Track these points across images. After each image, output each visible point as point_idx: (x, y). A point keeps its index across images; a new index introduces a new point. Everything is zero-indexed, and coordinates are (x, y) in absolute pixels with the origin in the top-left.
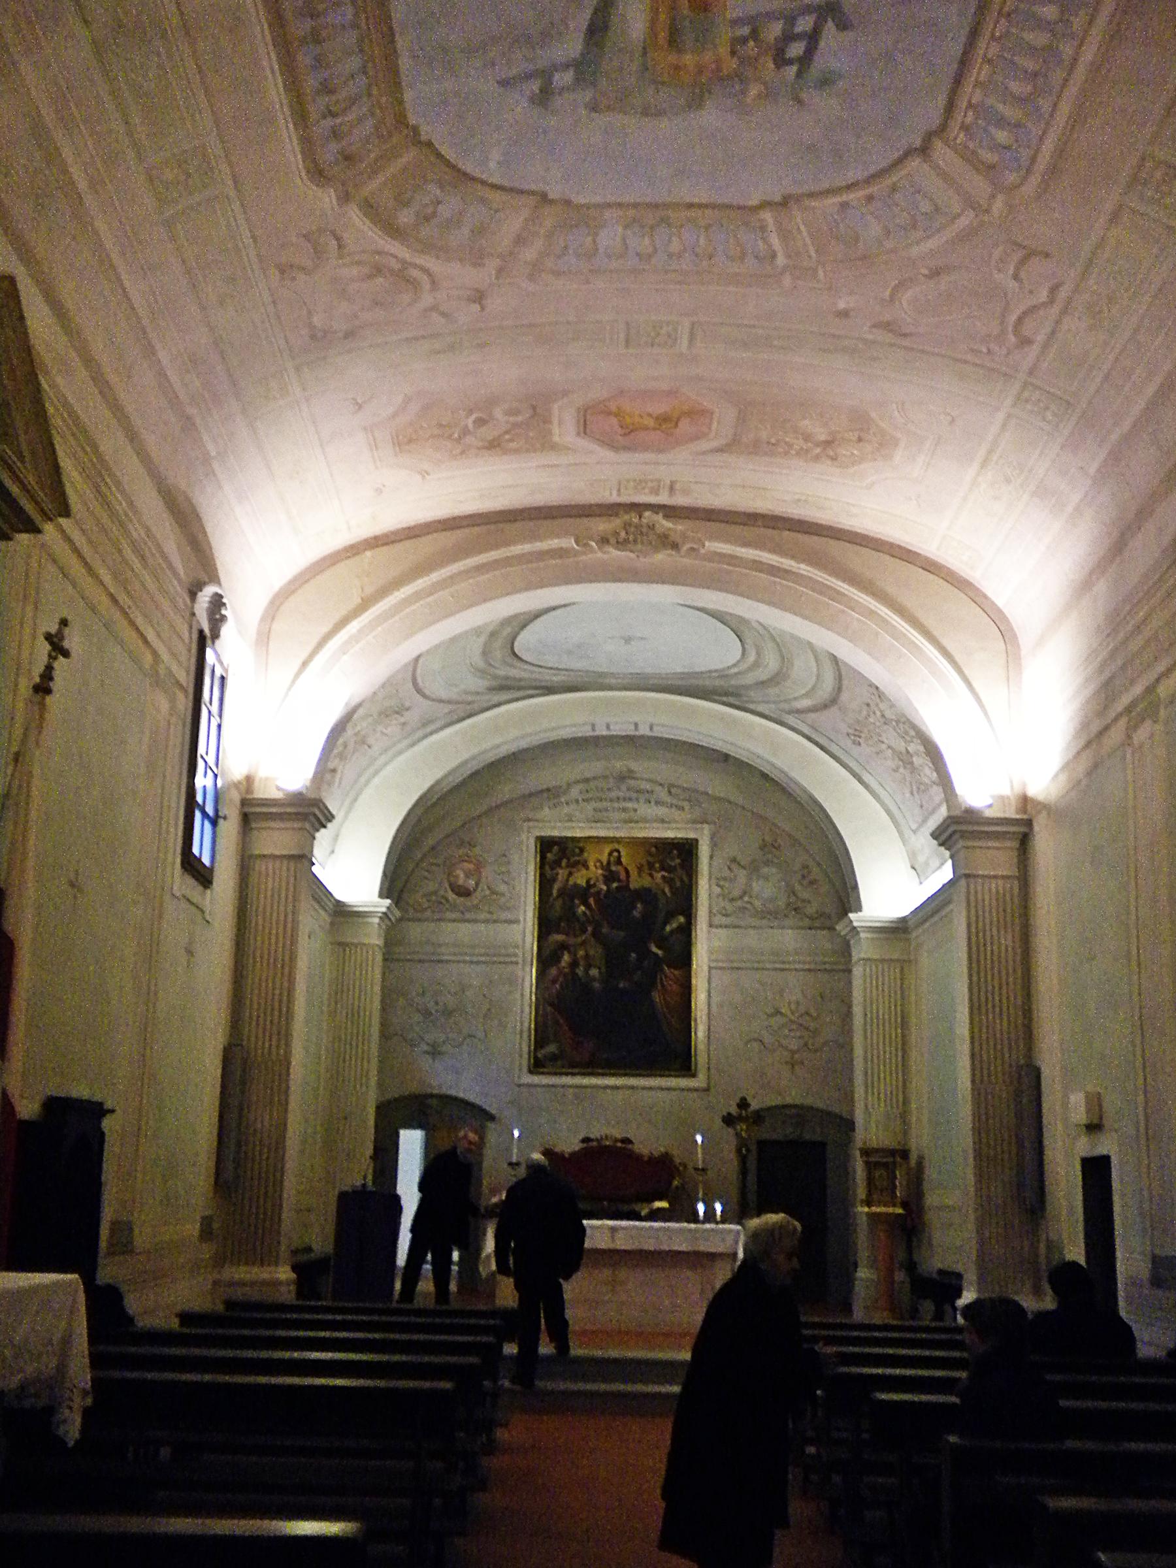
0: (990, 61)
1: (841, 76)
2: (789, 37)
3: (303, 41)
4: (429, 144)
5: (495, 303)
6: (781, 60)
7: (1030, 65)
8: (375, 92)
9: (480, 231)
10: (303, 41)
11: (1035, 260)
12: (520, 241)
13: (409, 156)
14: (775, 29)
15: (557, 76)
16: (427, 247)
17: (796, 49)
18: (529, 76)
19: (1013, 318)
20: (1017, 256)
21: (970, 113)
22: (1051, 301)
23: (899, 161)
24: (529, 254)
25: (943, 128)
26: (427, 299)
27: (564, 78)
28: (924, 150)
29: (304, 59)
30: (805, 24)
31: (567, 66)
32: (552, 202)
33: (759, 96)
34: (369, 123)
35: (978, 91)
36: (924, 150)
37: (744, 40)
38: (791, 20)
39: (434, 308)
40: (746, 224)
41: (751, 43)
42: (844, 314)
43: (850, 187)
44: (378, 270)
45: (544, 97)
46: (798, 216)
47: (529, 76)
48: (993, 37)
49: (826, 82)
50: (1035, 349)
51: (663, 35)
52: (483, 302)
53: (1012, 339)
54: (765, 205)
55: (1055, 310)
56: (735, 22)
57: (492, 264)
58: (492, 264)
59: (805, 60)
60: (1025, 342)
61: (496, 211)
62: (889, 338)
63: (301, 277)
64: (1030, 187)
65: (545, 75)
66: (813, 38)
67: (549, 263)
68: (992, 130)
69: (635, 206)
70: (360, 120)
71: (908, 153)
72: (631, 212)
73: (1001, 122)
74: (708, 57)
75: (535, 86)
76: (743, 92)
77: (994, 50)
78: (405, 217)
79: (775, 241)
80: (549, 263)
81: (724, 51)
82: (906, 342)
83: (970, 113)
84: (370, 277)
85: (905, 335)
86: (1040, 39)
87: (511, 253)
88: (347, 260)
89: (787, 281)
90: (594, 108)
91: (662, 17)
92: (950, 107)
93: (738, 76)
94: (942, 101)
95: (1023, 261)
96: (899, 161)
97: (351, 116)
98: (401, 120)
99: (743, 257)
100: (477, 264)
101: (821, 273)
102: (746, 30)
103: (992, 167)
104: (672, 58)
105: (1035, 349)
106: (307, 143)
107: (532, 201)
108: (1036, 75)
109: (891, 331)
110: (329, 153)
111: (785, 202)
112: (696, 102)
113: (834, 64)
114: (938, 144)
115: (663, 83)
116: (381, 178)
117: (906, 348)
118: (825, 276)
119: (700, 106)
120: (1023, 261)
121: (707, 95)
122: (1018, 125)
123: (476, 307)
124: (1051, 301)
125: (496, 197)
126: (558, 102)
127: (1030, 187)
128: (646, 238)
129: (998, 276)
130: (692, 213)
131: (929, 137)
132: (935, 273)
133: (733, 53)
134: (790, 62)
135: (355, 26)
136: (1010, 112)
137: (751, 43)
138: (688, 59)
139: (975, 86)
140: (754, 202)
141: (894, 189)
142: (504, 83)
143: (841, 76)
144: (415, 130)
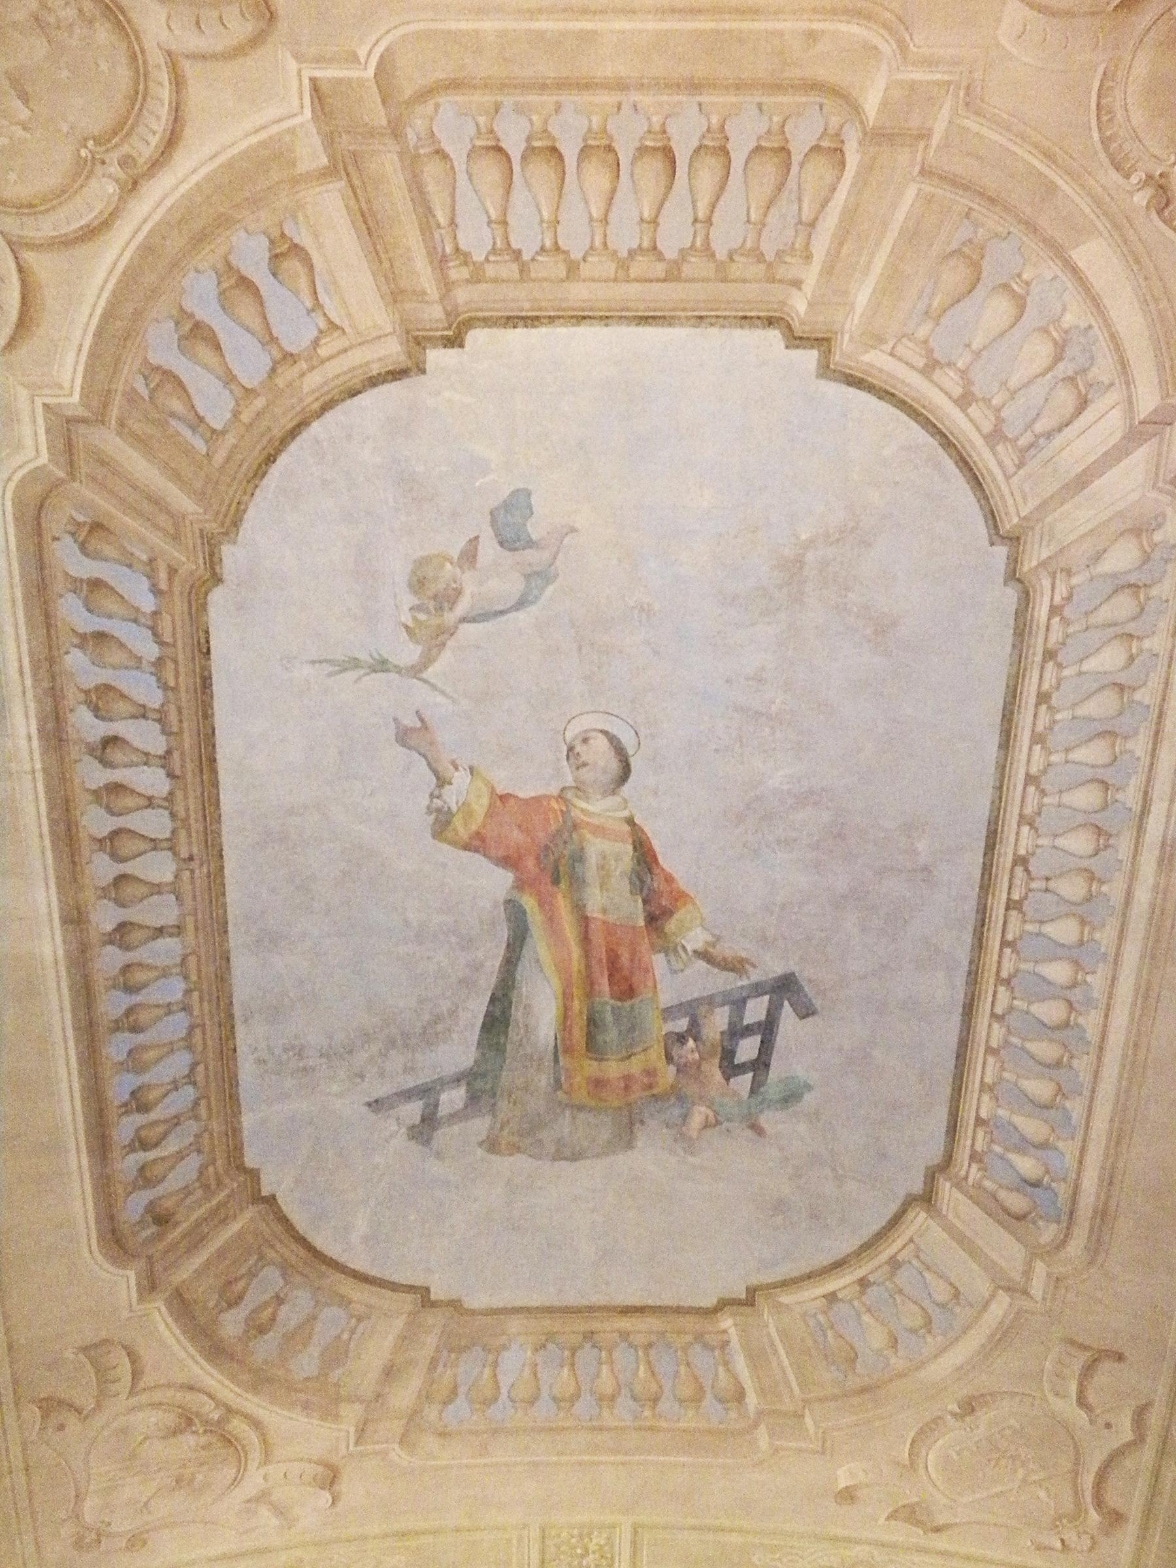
0: (1007, 982)
1: (809, 1088)
2: (736, 1032)
3: (117, 1027)
4: (272, 1200)
5: (352, 1488)
6: (731, 1068)
7: (1044, 1049)
8: (203, 1111)
9: (336, 1355)
10: (117, 1027)
11: (1106, 1365)
12: (390, 1373)
13: (245, 1219)
14: (718, 1022)
15: (444, 1097)
16: (259, 1381)
17: (747, 1049)
18: (408, 1095)
19: (1088, 1480)
20: (1080, 1360)
21: (980, 1133)
22: (1139, 1439)
23: (896, 1221)
24: (403, 1396)
25: (948, 1159)
26: (254, 1481)
27: (453, 1099)
28: (927, 1199)
29: (116, 1048)
30: (756, 1010)
31: (457, 1080)
32: (434, 1304)
33: (706, 1126)
34: (194, 1162)
35: (974, 1167)
36: (927, 1199)
37: (681, 1038)
38: (739, 1004)
39: (262, 1497)
40: (699, 1337)
41: (691, 1043)
42: (848, 1496)
43: (838, 1265)
44: (187, 1420)
45: (429, 1122)
46: (769, 1320)
47: (408, 1095)
48: (993, 1015)
49: (791, 1097)
50: (1131, 1529)
51: (578, 1035)
52: (336, 1487)
53: (1094, 1516)
54: (723, 1305)
55: (1147, 1454)
56: (668, 1013)
57: (351, 1413)
58: (351, 1413)
59: (761, 1064)
60: (1116, 1518)
61: (360, 1319)
62: (917, 1536)
63: (73, 1424)
64: (1076, 1247)
65: (427, 1092)
66: (768, 1029)
67: (431, 1413)
68: (1013, 1157)
69: (549, 1310)
70: (180, 1156)
71: (910, 1202)
72: (547, 1323)
73: (1024, 1145)
74: (635, 1066)
75: (413, 1110)
76: (685, 1117)
77: (998, 1031)
78: (231, 1324)
79: (741, 1365)
80: (431, 1413)
81: (655, 1055)
82: (941, 1542)
83: (980, 1133)
84: (175, 1432)
85: (938, 1530)
86: (1058, 972)
87: (379, 1396)
88: (144, 1398)
89: (762, 1434)
90: (492, 1145)
91: (576, 1005)
92: (952, 1129)
93: (676, 1094)
94: (941, 1114)
95: (1088, 1371)
96: (896, 1221)
97: (171, 1147)
98: (235, 1151)
99: (697, 1398)
100: (329, 1413)
101: (808, 1420)
102: (682, 1024)
103: (1020, 1218)
104: (591, 1068)
105: (1131, 1529)
106: (104, 1185)
107: (408, 1301)
108: (1058, 1064)
109: (918, 1523)
110: (134, 1206)
111: (750, 1299)
112: (625, 1137)
113: (800, 1071)
114: (945, 1189)
115: (581, 1108)
116: (197, 1261)
117: (943, 1554)
118: (817, 1427)
119: (630, 1145)
120: (1088, 1371)
121: (638, 1125)
122: (1043, 1146)
123: (327, 1496)
124: (1139, 1439)
125: (358, 1294)
126: (444, 1136)
127: (1076, 1247)
128: (566, 1370)
129: (1057, 1404)
130: (625, 1323)
131: (931, 1177)
132: (969, 1407)
133: (669, 1058)
134: (741, 1069)
135: (186, 1008)
136: (1032, 1127)
137: (691, 1043)
138: (613, 1069)
139: (1007, 908)
140: (709, 1302)
141: (895, 1264)
142: (376, 1105)
143: (809, 1088)
144: (254, 1175)
